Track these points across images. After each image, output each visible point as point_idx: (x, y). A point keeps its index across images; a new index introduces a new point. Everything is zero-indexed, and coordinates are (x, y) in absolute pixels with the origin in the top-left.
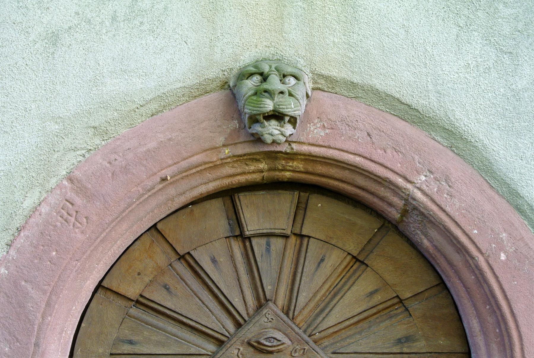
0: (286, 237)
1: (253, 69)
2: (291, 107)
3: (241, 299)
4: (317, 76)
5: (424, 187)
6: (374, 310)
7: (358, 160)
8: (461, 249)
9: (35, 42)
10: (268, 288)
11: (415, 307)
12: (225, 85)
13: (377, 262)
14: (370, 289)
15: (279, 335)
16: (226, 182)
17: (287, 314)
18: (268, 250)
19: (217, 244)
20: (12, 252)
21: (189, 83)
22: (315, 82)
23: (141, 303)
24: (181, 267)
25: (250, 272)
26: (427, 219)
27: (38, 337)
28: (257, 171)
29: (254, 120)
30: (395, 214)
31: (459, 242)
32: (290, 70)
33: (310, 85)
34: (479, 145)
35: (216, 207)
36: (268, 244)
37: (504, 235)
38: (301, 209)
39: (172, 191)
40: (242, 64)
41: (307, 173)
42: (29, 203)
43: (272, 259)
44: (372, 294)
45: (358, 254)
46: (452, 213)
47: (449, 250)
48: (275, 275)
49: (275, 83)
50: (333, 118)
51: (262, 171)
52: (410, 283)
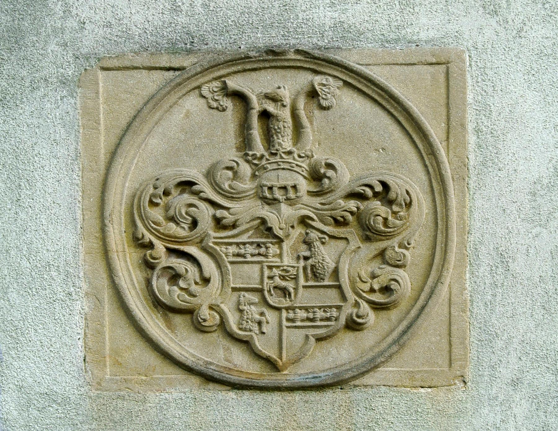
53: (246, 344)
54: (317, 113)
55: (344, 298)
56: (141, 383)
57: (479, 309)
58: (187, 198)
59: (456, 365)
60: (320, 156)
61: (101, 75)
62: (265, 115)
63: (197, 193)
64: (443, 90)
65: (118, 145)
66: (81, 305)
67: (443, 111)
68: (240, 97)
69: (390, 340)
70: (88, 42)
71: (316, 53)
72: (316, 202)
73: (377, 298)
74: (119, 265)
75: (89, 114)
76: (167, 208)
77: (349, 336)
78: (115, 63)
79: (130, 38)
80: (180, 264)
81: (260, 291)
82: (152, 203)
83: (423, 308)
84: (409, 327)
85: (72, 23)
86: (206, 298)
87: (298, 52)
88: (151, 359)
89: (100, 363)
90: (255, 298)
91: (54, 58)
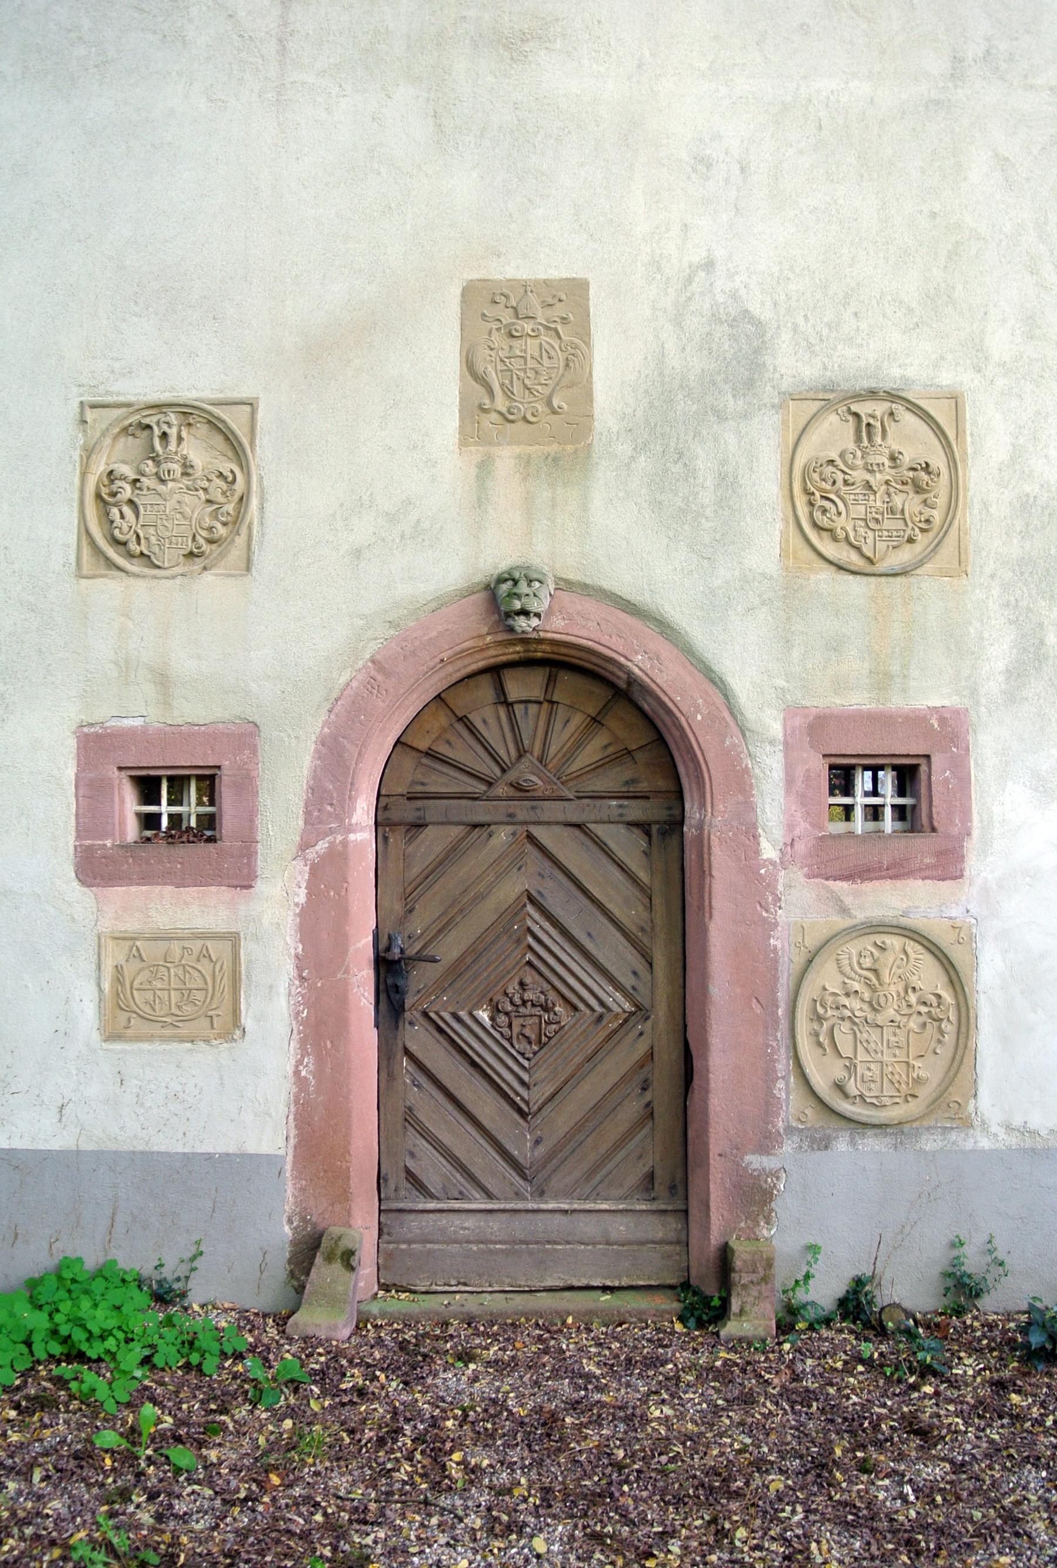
0: (540, 703)
1: (507, 576)
2: (534, 606)
3: (506, 750)
4: (558, 580)
5: (641, 665)
6: (608, 759)
7: (590, 644)
8: (669, 712)
9: (344, 557)
10: (526, 742)
11: (639, 756)
12: (487, 587)
13: (610, 722)
14: (606, 742)
15: (534, 778)
16: (492, 661)
17: (541, 762)
18: (526, 713)
19: (487, 709)
20: (332, 716)
21: (459, 586)
22: (557, 584)
23: (430, 754)
24: (459, 727)
25: (513, 730)
26: (644, 689)
27: (353, 778)
28: (515, 652)
29: (508, 615)
30: (623, 685)
31: (667, 707)
32: (535, 576)
33: (552, 587)
34: (683, 632)
35: (486, 681)
36: (526, 709)
37: (700, 701)
38: (551, 681)
39: (450, 669)
40: (500, 571)
41: (553, 653)
42: (343, 680)
43: (529, 720)
44: (606, 747)
45: (599, 714)
46: (661, 684)
47: (661, 712)
48: (531, 732)
49: (523, 588)
50: (571, 611)
51: (518, 652)
52: (636, 738)
53: (858, 549)
54: (893, 423)
55: (906, 525)
56: (807, 569)
57: (974, 533)
58: (831, 468)
59: (963, 564)
60: (896, 447)
61: (791, 402)
62: (869, 425)
63: (836, 466)
64: (954, 412)
65: (799, 439)
66: (779, 525)
67: (954, 423)
68: (856, 415)
69: (929, 549)
70: (786, 384)
71: (894, 392)
72: (893, 472)
73: (923, 525)
74: (798, 504)
75: (785, 422)
76: (821, 474)
77: (909, 545)
78: (798, 397)
79: (804, 383)
80: (827, 504)
81: (866, 520)
82: (814, 471)
83: (946, 532)
84: (939, 543)
85: (777, 376)
86: (840, 522)
87: (885, 392)
88: (812, 556)
89: (787, 557)
90: (862, 524)
91: (769, 394)
